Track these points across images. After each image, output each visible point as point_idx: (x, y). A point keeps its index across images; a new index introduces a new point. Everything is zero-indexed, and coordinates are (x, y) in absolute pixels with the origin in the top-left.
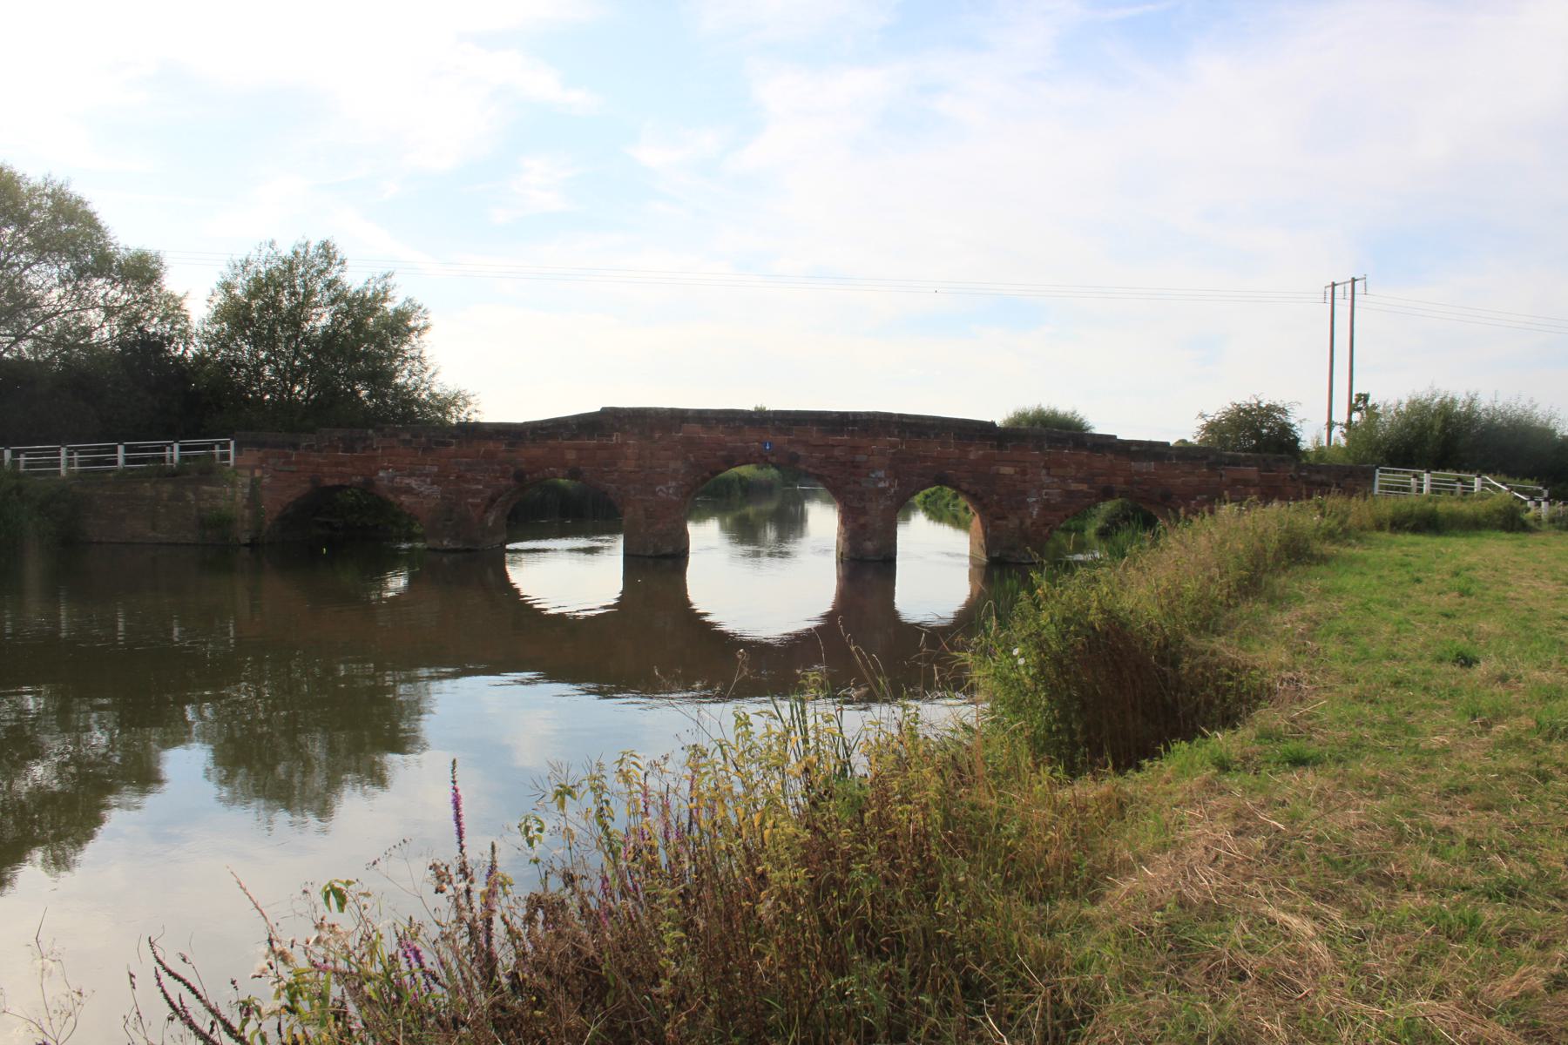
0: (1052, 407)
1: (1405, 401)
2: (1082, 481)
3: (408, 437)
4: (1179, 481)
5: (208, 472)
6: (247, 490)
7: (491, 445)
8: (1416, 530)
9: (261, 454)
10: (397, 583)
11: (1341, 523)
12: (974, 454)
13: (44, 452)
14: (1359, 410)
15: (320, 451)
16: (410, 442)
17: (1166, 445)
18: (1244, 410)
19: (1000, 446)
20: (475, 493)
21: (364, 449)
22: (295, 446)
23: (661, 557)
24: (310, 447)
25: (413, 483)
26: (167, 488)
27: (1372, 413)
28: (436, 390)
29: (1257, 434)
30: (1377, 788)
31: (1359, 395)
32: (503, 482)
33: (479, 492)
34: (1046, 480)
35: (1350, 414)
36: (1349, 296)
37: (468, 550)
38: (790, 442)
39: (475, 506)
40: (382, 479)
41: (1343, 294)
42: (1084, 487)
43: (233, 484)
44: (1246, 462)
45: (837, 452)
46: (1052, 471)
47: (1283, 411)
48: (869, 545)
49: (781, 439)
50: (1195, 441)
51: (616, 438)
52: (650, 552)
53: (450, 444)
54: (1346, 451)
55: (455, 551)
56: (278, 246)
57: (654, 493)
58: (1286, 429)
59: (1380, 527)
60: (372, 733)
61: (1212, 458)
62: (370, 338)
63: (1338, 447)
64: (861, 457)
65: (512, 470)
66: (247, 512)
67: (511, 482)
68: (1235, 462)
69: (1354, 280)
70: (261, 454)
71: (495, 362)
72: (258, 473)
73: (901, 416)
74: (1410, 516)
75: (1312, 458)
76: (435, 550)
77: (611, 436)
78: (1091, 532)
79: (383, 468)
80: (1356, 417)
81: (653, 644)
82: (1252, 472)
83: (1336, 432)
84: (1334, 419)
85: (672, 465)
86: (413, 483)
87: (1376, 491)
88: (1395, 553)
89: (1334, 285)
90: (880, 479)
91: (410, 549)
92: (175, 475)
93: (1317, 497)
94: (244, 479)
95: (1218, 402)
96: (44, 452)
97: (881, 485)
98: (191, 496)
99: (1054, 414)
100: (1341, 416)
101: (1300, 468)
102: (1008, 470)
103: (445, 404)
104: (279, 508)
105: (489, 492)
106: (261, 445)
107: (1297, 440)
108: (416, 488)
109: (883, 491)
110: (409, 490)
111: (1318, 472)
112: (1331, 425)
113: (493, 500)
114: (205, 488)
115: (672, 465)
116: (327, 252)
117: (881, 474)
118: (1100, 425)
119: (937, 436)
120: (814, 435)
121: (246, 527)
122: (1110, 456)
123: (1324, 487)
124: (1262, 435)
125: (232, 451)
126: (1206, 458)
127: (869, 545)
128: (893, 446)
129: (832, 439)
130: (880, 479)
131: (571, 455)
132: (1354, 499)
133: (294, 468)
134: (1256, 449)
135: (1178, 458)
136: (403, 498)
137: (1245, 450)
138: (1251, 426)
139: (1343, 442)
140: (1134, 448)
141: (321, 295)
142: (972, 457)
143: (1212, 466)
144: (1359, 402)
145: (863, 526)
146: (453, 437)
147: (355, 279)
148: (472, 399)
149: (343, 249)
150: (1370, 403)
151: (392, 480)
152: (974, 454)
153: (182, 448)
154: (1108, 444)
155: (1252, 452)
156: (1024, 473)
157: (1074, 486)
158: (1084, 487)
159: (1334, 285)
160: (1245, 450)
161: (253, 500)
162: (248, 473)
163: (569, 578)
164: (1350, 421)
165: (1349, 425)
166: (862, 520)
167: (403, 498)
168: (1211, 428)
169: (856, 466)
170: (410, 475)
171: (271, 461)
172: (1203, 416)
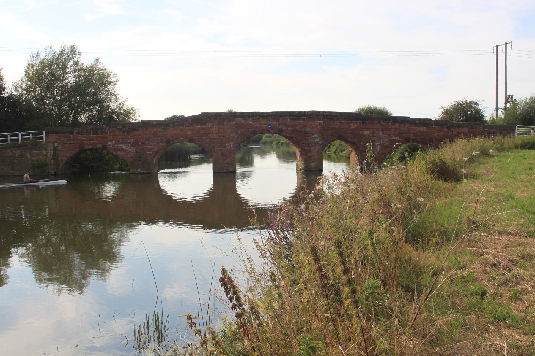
0: (367, 106)
1: (529, 97)
2: (397, 136)
3: (120, 127)
4: (436, 134)
5: (36, 145)
6: (52, 152)
7: (156, 130)
8: (530, 148)
9: (57, 137)
10: (109, 191)
11: (501, 146)
12: (353, 126)
13: (37, 134)
14: (509, 102)
15: (83, 134)
16: (121, 129)
17: (431, 120)
18: (460, 104)
19: (363, 123)
20: (150, 150)
21: (102, 133)
22: (72, 133)
23: (231, 172)
24: (78, 133)
25: (123, 146)
26: (18, 152)
27: (515, 103)
28: (125, 108)
29: (466, 114)
30: (496, 166)
31: (509, 96)
32: (162, 145)
33: (152, 149)
34: (383, 136)
35: (506, 104)
36: (504, 51)
37: (148, 173)
38: (279, 124)
39: (151, 155)
40: (110, 145)
41: (502, 50)
42: (398, 138)
43: (46, 150)
44: (463, 125)
45: (298, 128)
46: (385, 132)
47: (477, 104)
48: (313, 165)
49: (275, 123)
50: (439, 118)
51: (208, 125)
52: (225, 171)
53: (139, 130)
54: (504, 120)
55: (143, 174)
56: (53, 48)
57: (225, 147)
58: (478, 111)
59: (516, 147)
60: (100, 254)
61: (449, 124)
62: (93, 85)
63: (501, 119)
64: (308, 129)
65: (165, 139)
66: (53, 161)
67: (165, 144)
68: (458, 126)
69: (506, 44)
70: (57, 137)
71: (147, 95)
72: (56, 145)
73: (323, 112)
74: (528, 143)
75: (490, 124)
76: (134, 174)
77: (205, 124)
78: (395, 159)
79: (111, 141)
80: (508, 105)
81: (223, 210)
82: (465, 129)
83: (499, 112)
84: (499, 106)
85: (232, 135)
86: (123, 146)
87: (516, 135)
88: (521, 154)
89: (497, 46)
90: (316, 138)
91: (114, 174)
92: (21, 147)
93: (492, 137)
94: (51, 147)
95: (448, 102)
96: (37, 134)
97: (317, 140)
98: (28, 155)
99: (375, 108)
100: (501, 105)
101: (485, 127)
102: (366, 132)
103: (128, 113)
104: (66, 159)
105: (156, 149)
106: (57, 133)
107: (483, 116)
108: (126, 149)
109: (317, 142)
110: (121, 149)
111: (492, 128)
112: (497, 109)
113: (157, 152)
114: (34, 152)
115: (232, 135)
116: (73, 49)
117: (316, 136)
118: (396, 112)
119: (338, 119)
120: (289, 121)
121: (53, 167)
122: (408, 125)
123: (494, 134)
124: (468, 114)
125: (44, 135)
126: (446, 124)
127: (313, 165)
128: (321, 124)
129: (296, 122)
130: (316, 138)
131: (189, 133)
132: (506, 138)
133: (72, 142)
134: (465, 120)
135: (435, 125)
136: (119, 153)
137: (461, 121)
138: (463, 111)
139: (503, 116)
140: (417, 122)
141: (70, 68)
142: (352, 127)
143: (449, 128)
144: (509, 98)
145: (310, 157)
146: (140, 127)
147: (86, 61)
148: (137, 111)
149: (80, 47)
150: (514, 99)
151: (114, 145)
152: (353, 126)
153: (22, 135)
154: (405, 120)
155: (464, 120)
156: (374, 133)
157: (393, 138)
158: (398, 138)
159: (497, 46)
160: (461, 121)
161: (55, 156)
162: (52, 144)
163: (192, 182)
164: (506, 107)
165: (505, 108)
166: (309, 155)
167: (119, 153)
168: (446, 112)
169: (306, 133)
170: (122, 143)
171: (62, 139)
172: (442, 107)
